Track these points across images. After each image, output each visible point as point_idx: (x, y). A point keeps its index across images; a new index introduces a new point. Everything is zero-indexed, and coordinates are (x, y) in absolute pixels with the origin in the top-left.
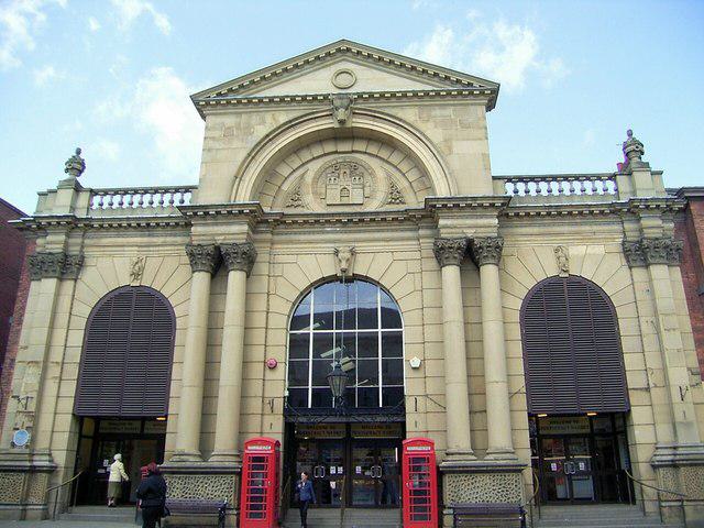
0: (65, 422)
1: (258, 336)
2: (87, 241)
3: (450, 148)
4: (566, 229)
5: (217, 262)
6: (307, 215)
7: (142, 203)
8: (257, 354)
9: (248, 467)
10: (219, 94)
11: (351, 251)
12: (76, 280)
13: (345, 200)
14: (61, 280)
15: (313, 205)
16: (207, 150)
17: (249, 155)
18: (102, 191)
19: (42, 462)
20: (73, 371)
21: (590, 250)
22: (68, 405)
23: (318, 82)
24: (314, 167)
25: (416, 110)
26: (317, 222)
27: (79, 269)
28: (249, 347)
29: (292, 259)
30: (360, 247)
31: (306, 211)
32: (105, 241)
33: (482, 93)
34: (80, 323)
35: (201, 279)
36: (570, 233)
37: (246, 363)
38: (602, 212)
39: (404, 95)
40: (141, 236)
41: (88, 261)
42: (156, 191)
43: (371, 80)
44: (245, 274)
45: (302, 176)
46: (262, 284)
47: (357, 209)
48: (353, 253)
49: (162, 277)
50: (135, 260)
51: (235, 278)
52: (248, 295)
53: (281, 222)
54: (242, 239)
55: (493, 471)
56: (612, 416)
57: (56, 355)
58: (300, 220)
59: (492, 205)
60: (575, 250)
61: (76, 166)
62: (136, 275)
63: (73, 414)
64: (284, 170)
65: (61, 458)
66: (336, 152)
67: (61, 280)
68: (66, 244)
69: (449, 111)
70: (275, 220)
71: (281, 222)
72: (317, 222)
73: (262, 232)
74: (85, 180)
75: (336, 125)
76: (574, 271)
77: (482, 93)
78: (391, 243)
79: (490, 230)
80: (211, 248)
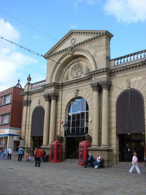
0: (29, 137)
1: (59, 116)
2: (31, 96)
3: (96, 55)
4: (130, 73)
5: (99, 88)
6: (69, 82)
7: (128, 60)
8: (59, 120)
9: (52, 149)
10: (48, 54)
11: (77, 90)
12: (30, 106)
13: (77, 76)
14: (27, 106)
15: (71, 79)
16: (47, 70)
17: (53, 69)
18: (140, 52)
19: (26, 146)
20: (30, 127)
21: (137, 79)
22: (30, 134)
23: (68, 44)
24: (70, 69)
25: (88, 45)
26: (71, 83)
27: (30, 104)
28: (110, 113)
29: (66, 94)
30: (80, 89)
31: (70, 81)
32: (34, 96)
33: (103, 35)
34: (31, 116)
35: (96, 94)
36: (131, 74)
37: (56, 123)
38: (139, 65)
39: (89, 40)
40: (89, 82)
41: (32, 101)
42: (118, 59)
43: (80, 39)
44: (107, 91)
45: (69, 70)
46: (60, 102)
47: (80, 78)
48: (78, 91)
49: (43, 103)
50: (39, 99)
51: (105, 92)
52: (56, 105)
53: (63, 85)
54: (105, 80)
55: (100, 150)
56: (40, 137)
57: (27, 124)
58: (66, 84)
59: (103, 71)
60: (133, 80)
61: (29, 79)
62: (39, 103)
63: (116, 134)
64: (64, 71)
65: (29, 146)
66: (75, 62)
67: (27, 106)
68: (28, 98)
69: (96, 43)
70: (61, 85)
71: (63, 85)
72: (71, 83)
73: (60, 88)
74: (32, 82)
75: (71, 56)
76: (132, 87)
77: (103, 35)
78: (86, 86)
79: (104, 79)
80: (97, 84)
